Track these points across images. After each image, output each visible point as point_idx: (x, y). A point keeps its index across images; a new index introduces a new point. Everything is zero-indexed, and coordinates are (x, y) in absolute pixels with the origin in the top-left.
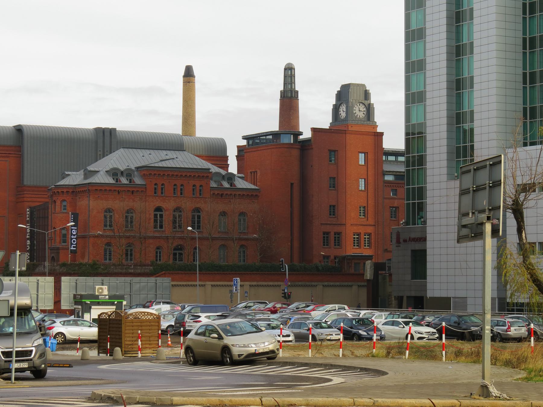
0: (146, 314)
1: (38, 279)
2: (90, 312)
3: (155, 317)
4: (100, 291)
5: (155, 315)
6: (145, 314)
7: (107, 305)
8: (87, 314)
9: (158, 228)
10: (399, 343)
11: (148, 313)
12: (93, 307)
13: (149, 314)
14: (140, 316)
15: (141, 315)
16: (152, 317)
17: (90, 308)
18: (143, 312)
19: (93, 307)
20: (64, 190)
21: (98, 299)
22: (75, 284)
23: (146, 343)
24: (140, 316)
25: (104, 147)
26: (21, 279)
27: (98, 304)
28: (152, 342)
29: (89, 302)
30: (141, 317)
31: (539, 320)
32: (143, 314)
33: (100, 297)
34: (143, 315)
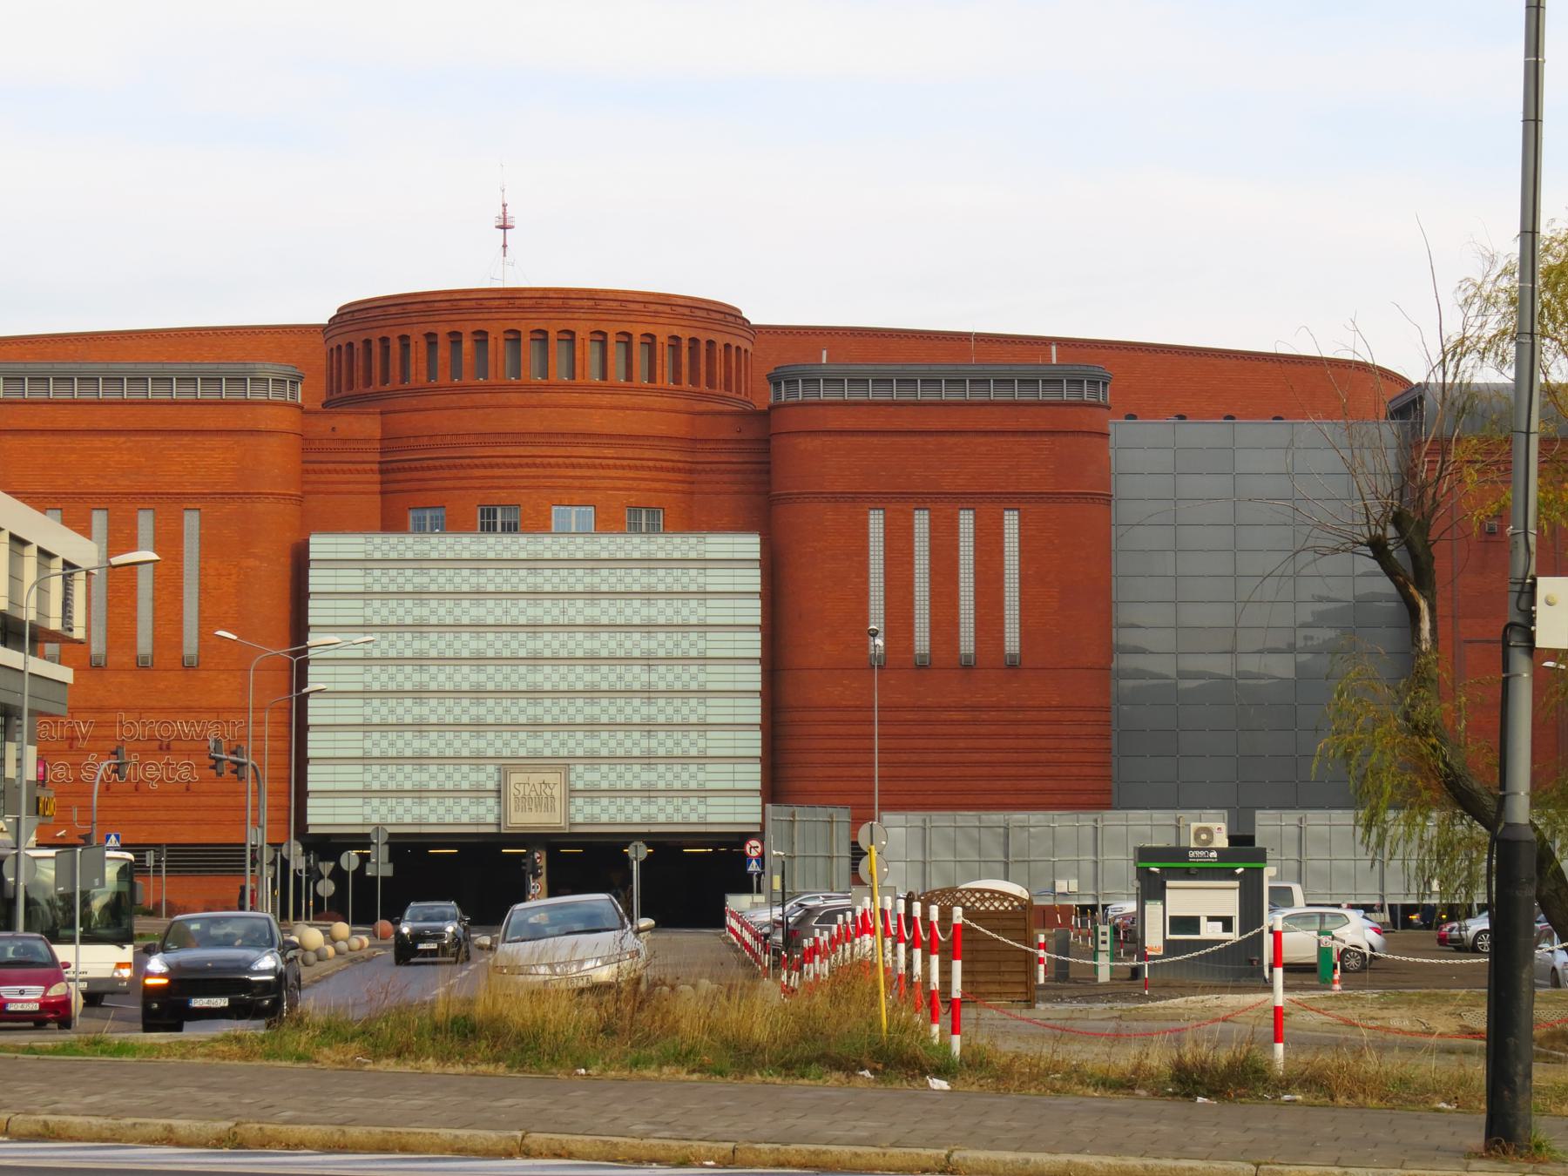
0: (987, 895)
1: (1178, 816)
2: (1162, 898)
3: (1016, 904)
4: (1204, 837)
5: (1016, 898)
6: (982, 895)
7: (1214, 878)
8: (1153, 902)
9: (378, 384)
10: (1552, 1048)
11: (992, 892)
12: (1169, 883)
13: (987, 895)
14: (968, 900)
15: (973, 899)
16: (1006, 904)
17: (1164, 887)
18: (978, 890)
19: (1169, 883)
20: (718, 335)
21: (1186, 859)
22: (1296, 830)
23: (989, 978)
24: (968, 900)
25: (1537, 121)
26: (1154, 816)
27: (1187, 874)
28: (1007, 977)
29: (1156, 870)
30: (973, 903)
31: (1557, 284)
32: (978, 895)
33: (1192, 854)
34: (977, 899)
